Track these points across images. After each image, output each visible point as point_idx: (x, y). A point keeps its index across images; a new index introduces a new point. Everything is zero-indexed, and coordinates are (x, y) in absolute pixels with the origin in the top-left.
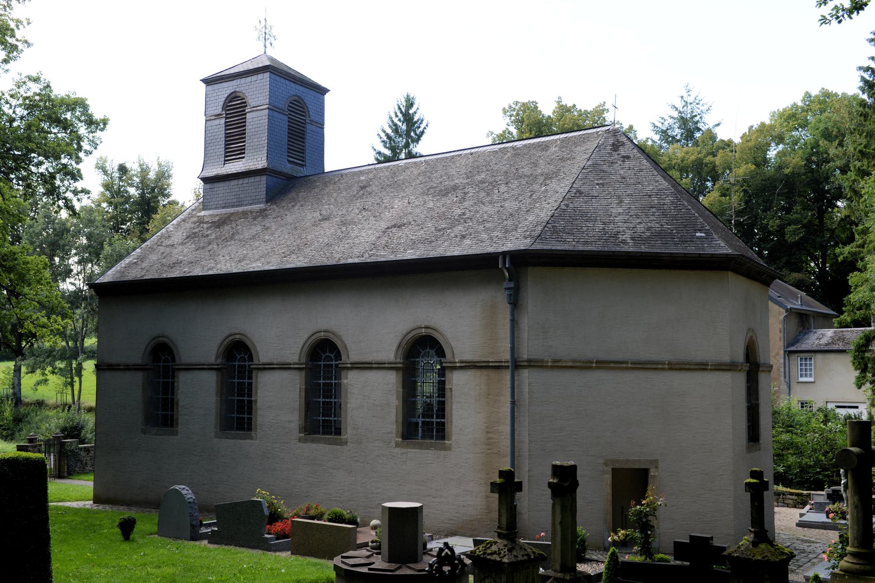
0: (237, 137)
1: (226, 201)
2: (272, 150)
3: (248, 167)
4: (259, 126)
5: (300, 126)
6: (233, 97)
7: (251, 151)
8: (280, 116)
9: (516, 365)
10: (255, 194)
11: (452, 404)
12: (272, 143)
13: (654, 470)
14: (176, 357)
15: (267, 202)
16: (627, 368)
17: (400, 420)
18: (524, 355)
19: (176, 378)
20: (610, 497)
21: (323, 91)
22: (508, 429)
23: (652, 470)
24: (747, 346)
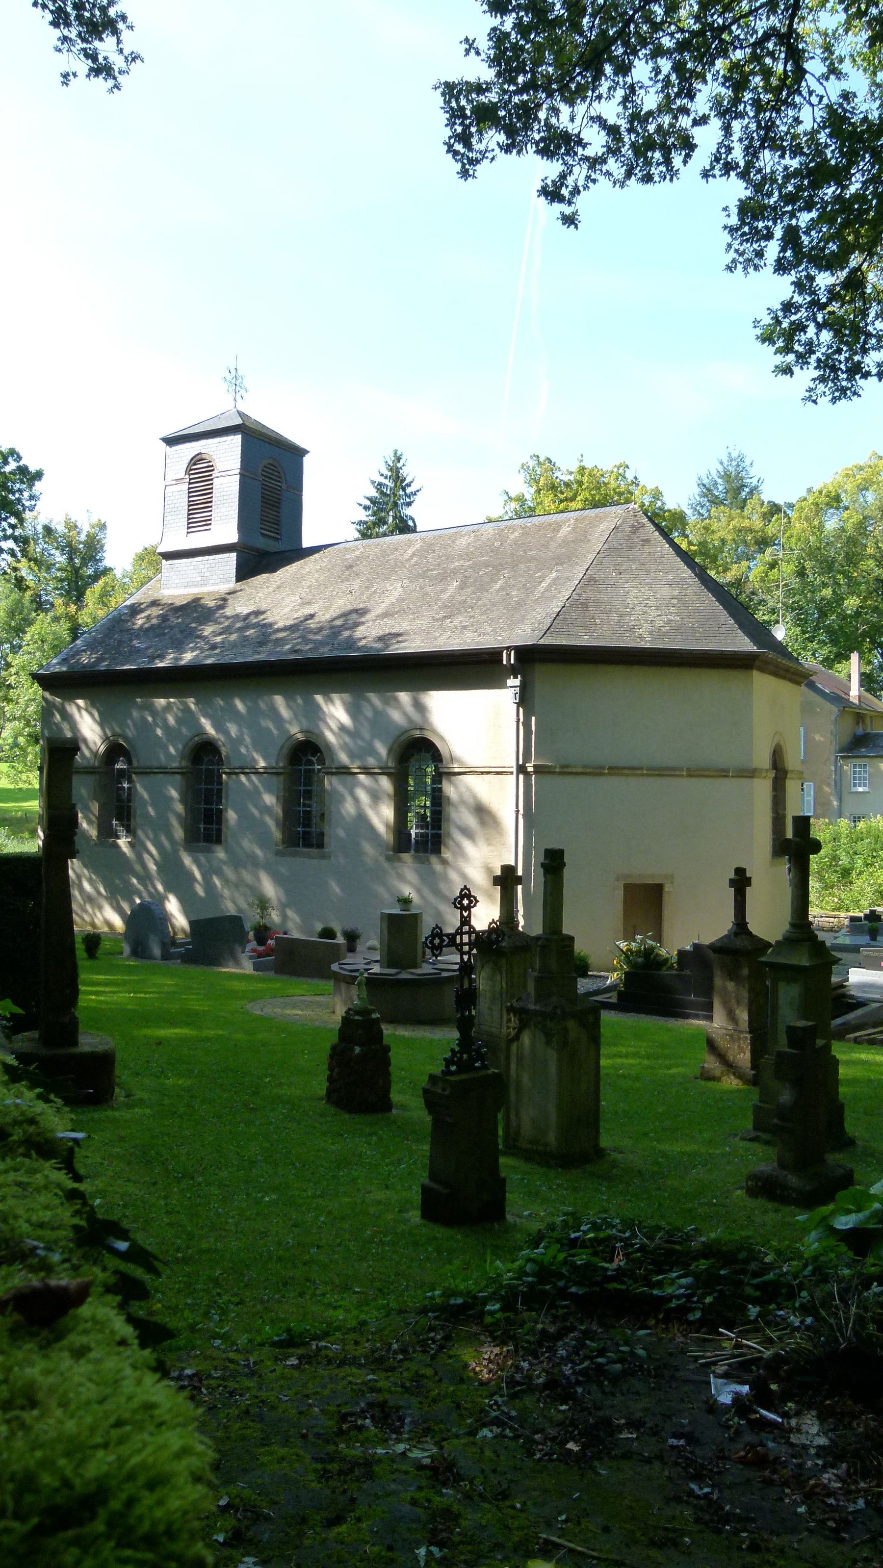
6: (197, 459)
10: (223, 572)
15: (237, 581)
16: (642, 775)
24: (774, 751)
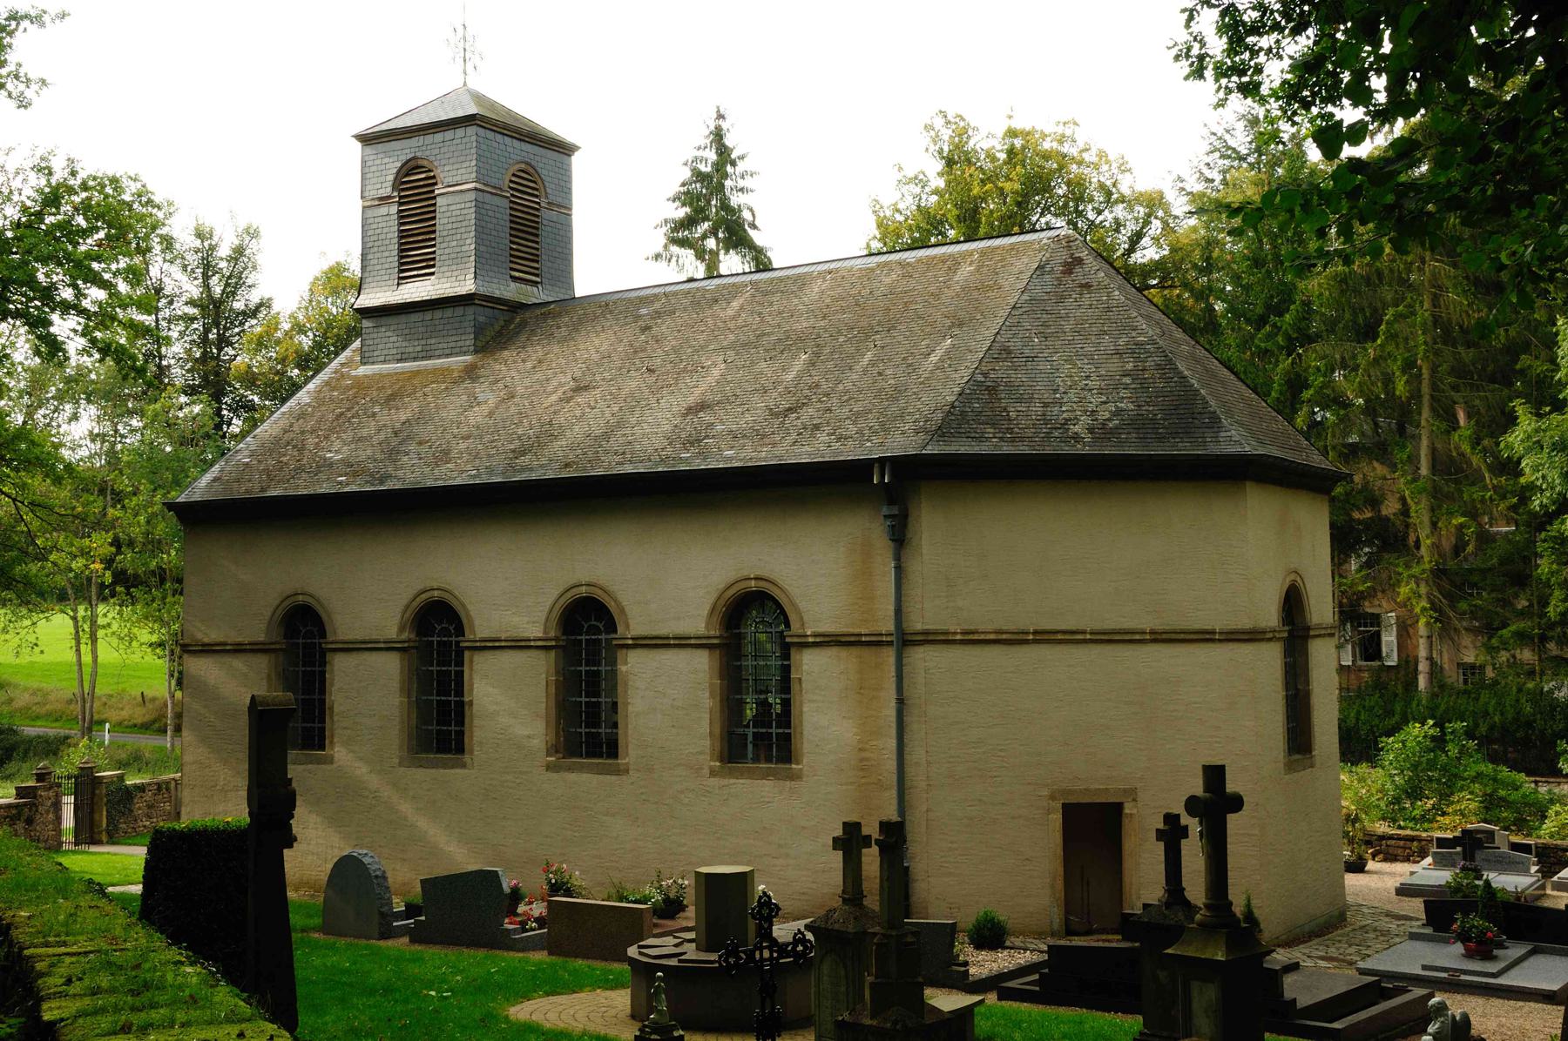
0: (420, 238)
1: (403, 350)
2: (484, 261)
3: (442, 292)
4: (460, 219)
5: (530, 227)
6: (410, 167)
7: (447, 263)
8: (497, 200)
9: (905, 640)
11: (801, 705)
12: (482, 248)
13: (1132, 804)
14: (327, 628)
16: (1085, 641)
17: (717, 731)
18: (916, 623)
19: (327, 665)
20: (1060, 852)
21: (564, 149)
22: (892, 743)
23: (1126, 805)
